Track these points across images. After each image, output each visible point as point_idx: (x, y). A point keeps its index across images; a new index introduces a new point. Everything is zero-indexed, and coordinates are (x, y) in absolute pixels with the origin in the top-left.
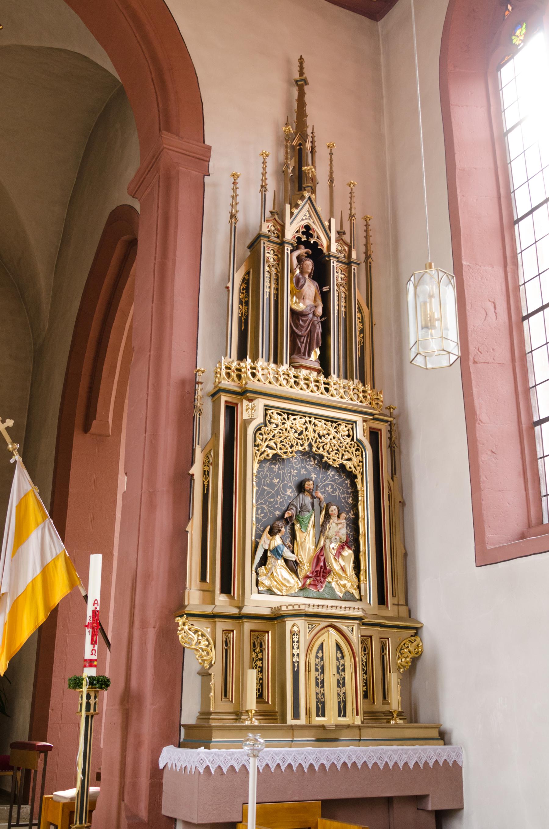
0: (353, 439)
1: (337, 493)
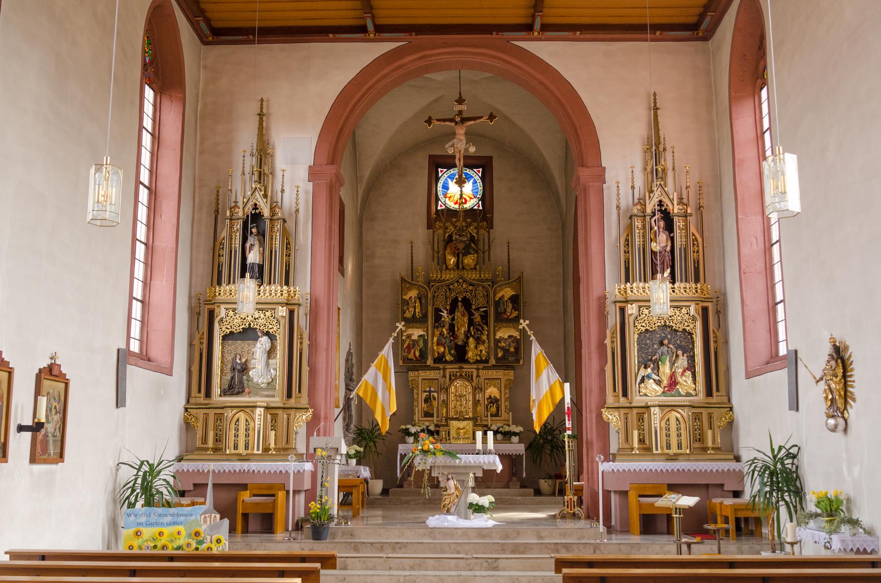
0: (690, 315)
1: (683, 343)
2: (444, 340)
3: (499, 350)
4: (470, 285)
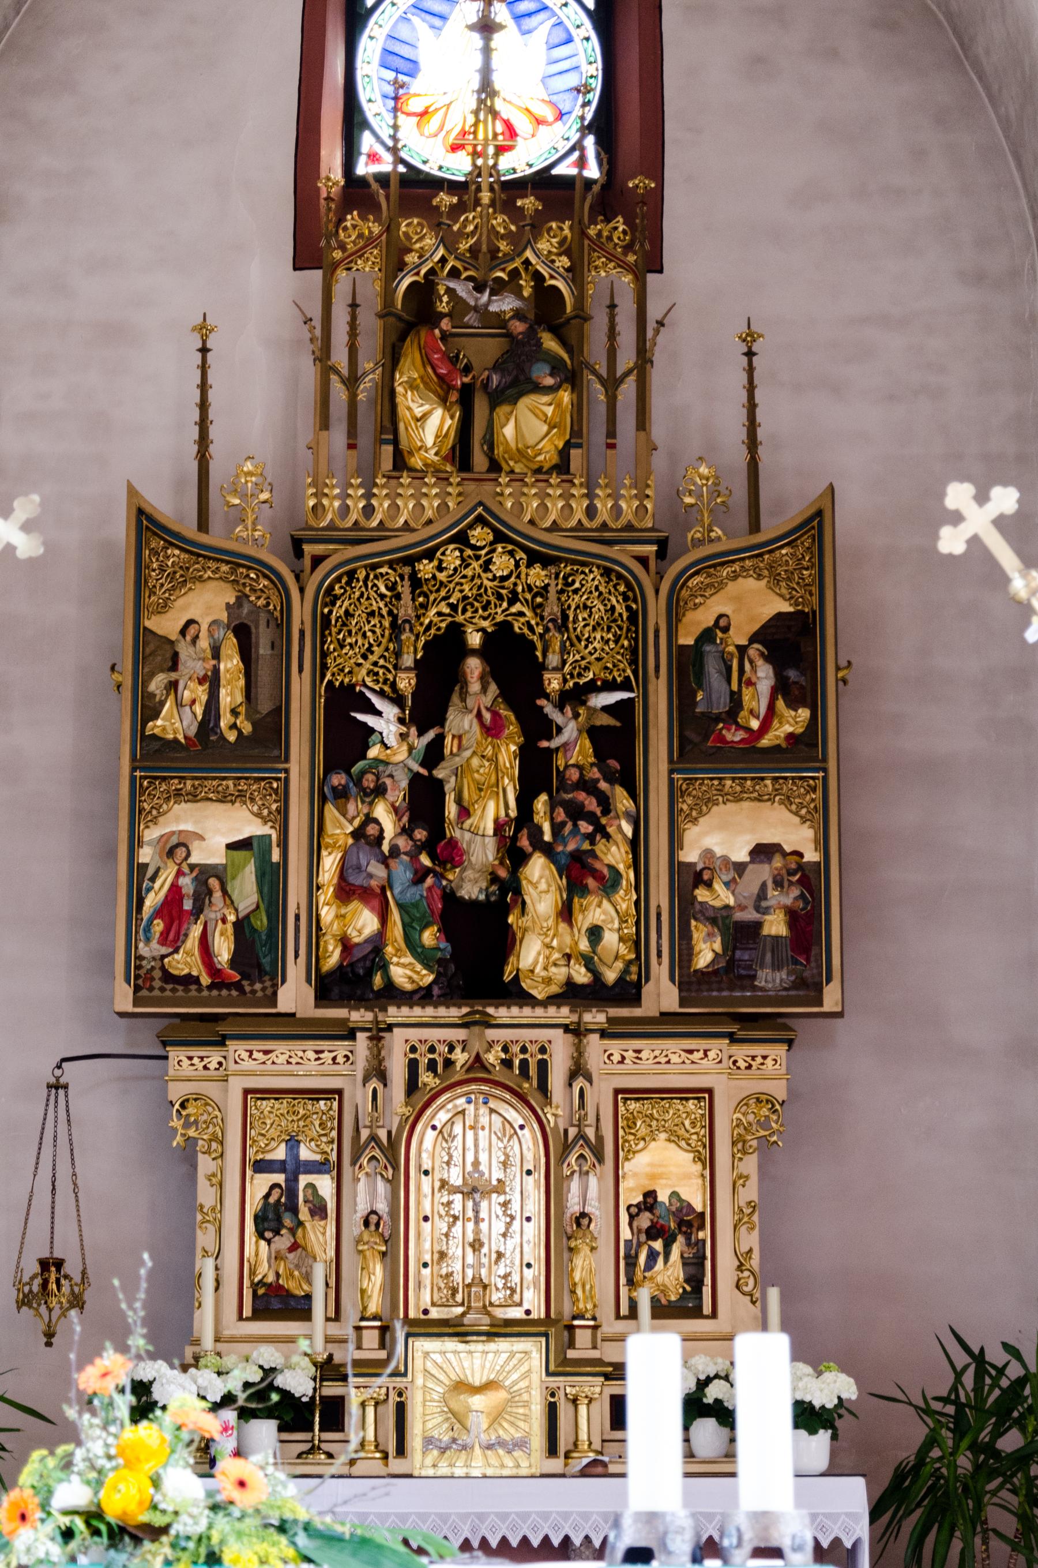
2: (378, 870)
3: (699, 931)
4: (534, 558)
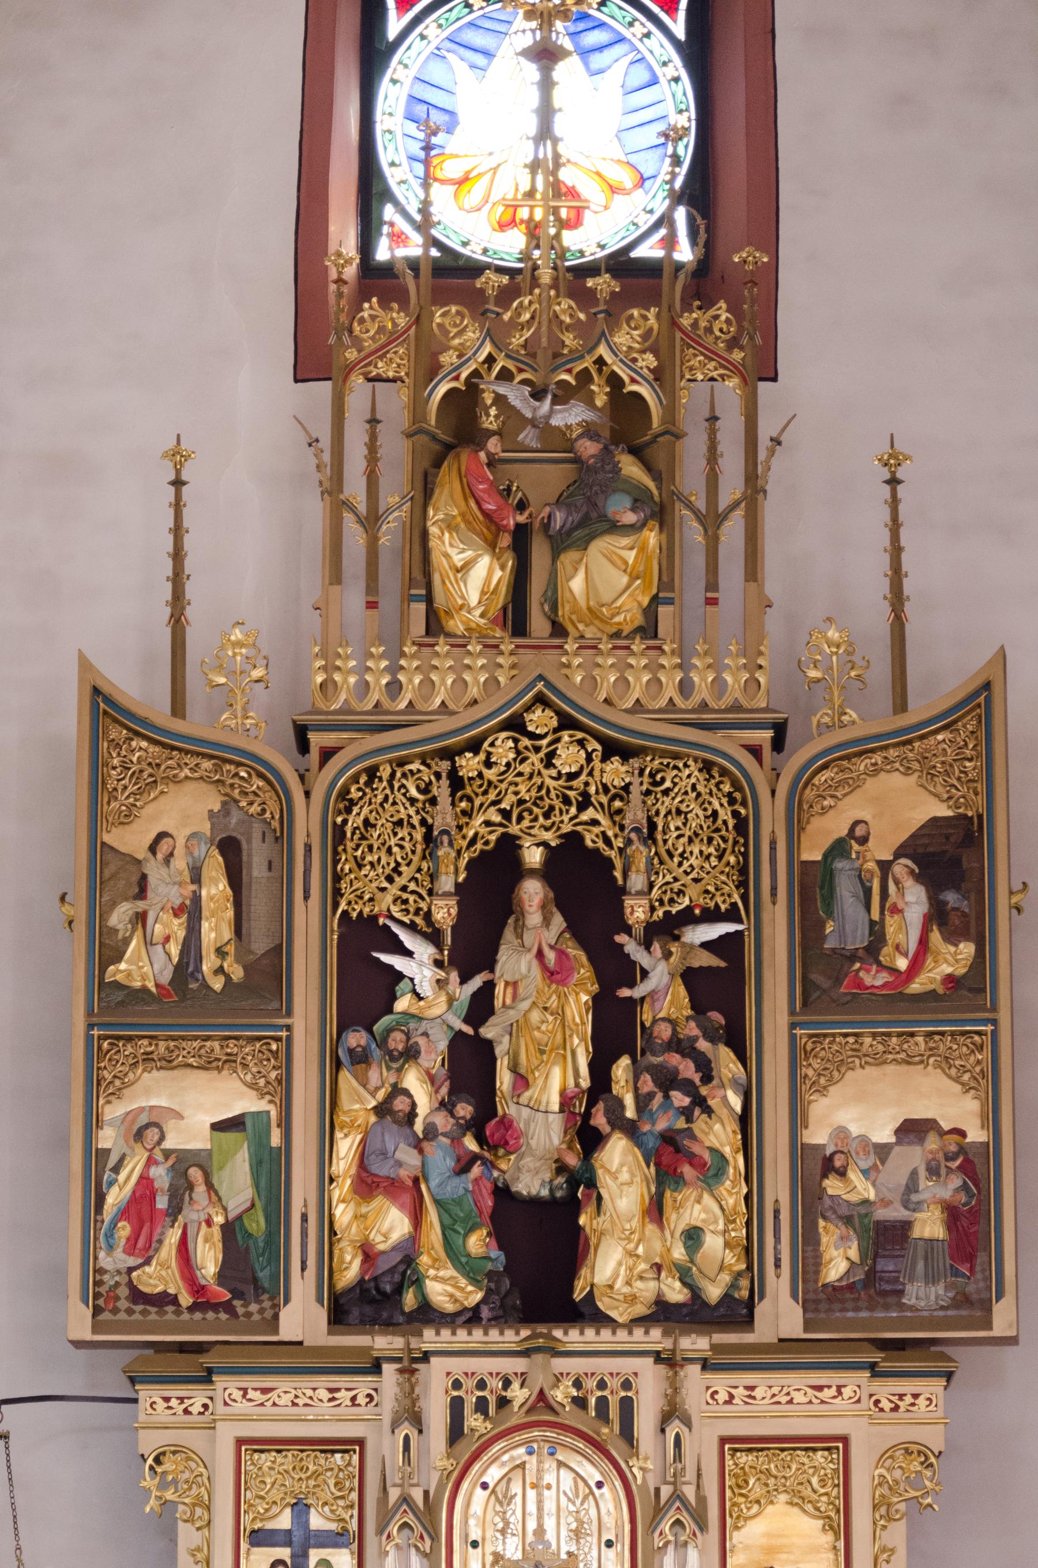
3: (829, 1234)
4: (612, 749)
